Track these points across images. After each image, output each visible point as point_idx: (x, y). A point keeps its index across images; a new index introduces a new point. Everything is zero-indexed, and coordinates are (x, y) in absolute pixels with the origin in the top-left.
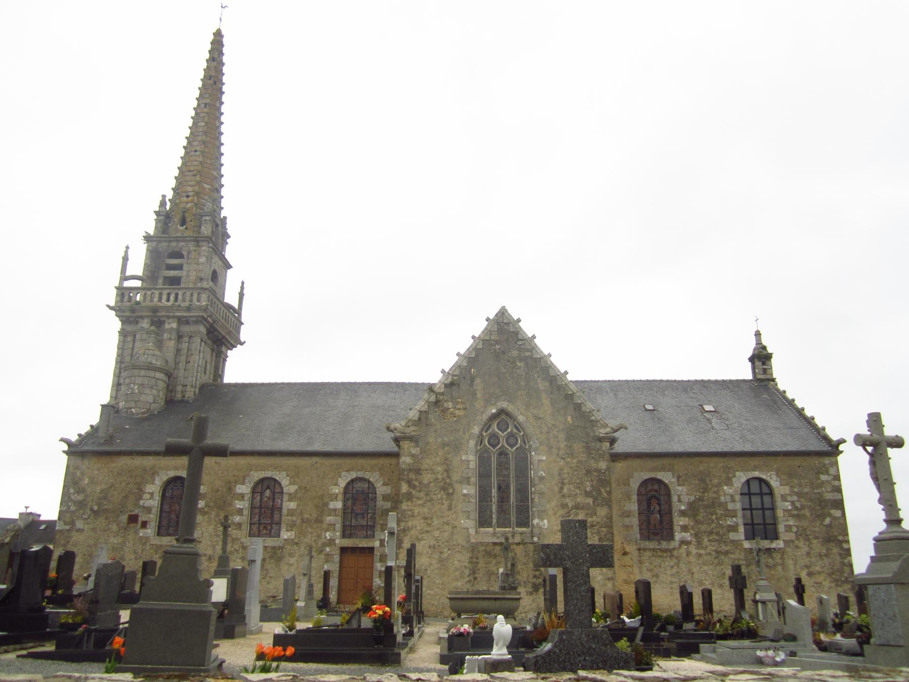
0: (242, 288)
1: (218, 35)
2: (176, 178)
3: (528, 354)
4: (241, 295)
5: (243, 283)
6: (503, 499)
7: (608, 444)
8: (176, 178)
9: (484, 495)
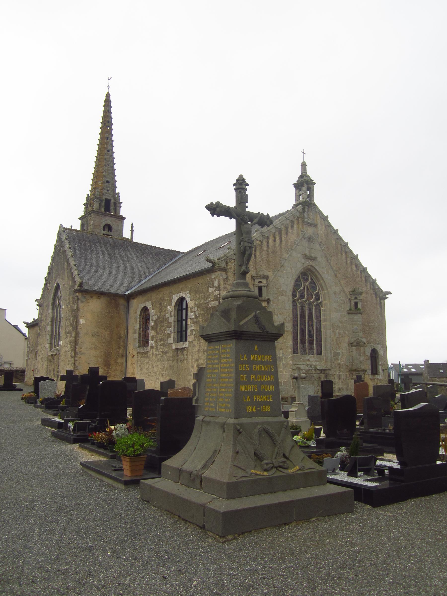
0: (132, 227)
1: (108, 96)
2: (100, 128)
3: (312, 375)
4: (132, 231)
5: (132, 224)
6: (303, 335)
7: (266, 303)
8: (100, 128)
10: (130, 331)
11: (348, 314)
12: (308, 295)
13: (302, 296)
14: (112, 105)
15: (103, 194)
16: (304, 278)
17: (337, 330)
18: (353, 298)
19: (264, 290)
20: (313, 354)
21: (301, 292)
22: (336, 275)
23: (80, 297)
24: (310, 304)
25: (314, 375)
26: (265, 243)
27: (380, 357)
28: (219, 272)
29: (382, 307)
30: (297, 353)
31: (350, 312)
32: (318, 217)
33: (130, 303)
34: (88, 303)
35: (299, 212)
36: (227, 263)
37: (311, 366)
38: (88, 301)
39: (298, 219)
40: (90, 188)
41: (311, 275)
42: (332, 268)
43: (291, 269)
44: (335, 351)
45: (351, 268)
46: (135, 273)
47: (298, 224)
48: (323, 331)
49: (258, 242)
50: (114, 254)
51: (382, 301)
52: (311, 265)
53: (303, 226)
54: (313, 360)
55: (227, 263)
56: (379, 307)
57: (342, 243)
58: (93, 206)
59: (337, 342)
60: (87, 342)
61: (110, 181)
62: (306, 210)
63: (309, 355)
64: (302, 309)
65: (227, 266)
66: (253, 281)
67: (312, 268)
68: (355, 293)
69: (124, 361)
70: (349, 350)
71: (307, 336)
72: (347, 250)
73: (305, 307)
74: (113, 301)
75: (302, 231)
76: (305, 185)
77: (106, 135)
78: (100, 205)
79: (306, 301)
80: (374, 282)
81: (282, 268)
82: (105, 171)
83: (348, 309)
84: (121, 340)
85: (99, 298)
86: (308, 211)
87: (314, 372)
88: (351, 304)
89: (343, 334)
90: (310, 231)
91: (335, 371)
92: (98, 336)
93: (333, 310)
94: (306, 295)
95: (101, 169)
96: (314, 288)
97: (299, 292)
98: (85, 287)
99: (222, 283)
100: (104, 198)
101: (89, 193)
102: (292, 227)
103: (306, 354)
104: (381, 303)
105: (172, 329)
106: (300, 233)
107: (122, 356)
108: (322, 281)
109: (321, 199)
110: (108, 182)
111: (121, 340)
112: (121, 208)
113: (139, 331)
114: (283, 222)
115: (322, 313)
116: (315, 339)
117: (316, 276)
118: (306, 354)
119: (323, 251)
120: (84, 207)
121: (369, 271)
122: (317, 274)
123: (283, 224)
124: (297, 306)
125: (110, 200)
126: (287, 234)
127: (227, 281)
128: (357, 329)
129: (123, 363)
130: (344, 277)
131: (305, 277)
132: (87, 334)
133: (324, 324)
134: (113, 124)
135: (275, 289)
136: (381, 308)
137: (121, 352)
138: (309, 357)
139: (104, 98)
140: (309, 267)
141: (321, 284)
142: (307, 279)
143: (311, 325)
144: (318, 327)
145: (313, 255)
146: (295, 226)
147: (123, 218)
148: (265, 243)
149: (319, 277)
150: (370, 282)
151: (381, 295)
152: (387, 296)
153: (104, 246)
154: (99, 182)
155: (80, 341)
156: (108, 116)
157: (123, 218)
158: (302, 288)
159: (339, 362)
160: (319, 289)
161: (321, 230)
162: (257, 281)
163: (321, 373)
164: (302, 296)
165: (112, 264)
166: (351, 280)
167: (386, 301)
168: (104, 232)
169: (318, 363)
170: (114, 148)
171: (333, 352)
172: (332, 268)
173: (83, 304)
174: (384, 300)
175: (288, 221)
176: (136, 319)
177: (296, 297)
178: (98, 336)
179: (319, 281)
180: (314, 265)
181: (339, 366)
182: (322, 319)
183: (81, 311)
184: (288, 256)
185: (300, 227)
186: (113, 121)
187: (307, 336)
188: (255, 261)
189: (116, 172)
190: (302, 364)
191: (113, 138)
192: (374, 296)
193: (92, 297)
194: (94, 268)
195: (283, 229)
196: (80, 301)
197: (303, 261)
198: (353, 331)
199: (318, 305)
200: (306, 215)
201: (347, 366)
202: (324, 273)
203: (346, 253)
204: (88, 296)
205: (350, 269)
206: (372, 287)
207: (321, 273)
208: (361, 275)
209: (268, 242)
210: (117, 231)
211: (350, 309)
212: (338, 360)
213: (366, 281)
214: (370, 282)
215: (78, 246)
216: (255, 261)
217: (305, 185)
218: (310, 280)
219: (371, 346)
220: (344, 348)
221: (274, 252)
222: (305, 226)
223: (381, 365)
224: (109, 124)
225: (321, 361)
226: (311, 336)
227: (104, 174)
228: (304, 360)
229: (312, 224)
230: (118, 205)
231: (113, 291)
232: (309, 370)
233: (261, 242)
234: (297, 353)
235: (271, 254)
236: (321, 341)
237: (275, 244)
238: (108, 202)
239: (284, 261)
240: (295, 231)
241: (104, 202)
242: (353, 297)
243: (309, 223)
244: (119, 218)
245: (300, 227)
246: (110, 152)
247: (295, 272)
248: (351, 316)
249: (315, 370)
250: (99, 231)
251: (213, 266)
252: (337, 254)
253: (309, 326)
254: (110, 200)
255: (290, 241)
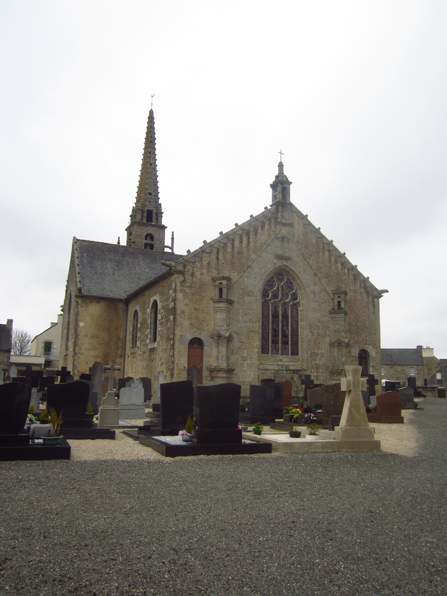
0: (173, 235)
1: (151, 112)
3: (282, 375)
4: (173, 239)
5: (173, 233)
6: (275, 335)
9: (264, 339)
10: (128, 333)
11: (331, 313)
12: (282, 295)
13: (275, 296)
14: (155, 121)
15: (145, 206)
16: (278, 278)
17: (315, 330)
18: (336, 297)
19: (224, 291)
20: (287, 354)
21: (274, 293)
22: (316, 274)
23: (79, 302)
24: (285, 304)
25: (285, 375)
26: (229, 245)
27: (371, 358)
28: (176, 275)
29: (376, 307)
30: (268, 353)
31: (333, 312)
32: (295, 216)
33: (129, 306)
34: (88, 307)
35: (272, 213)
36: (185, 266)
37: (282, 366)
38: (88, 305)
39: (270, 219)
40: (135, 200)
41: (286, 275)
42: (311, 267)
43: (260, 270)
44: (312, 351)
45: (336, 267)
46: (139, 279)
47: (270, 224)
48: (301, 331)
49: (221, 244)
50: (122, 261)
51: (376, 300)
52: (285, 265)
53: (275, 226)
54: (286, 361)
55: (185, 266)
56: (371, 306)
57: (325, 242)
58: (136, 218)
59: (315, 342)
60: (86, 343)
61: (153, 192)
62: (280, 210)
63: (282, 355)
64: (275, 308)
65: (184, 268)
66: (214, 282)
67: (286, 268)
68: (340, 293)
69: (123, 362)
70: (331, 350)
71: (280, 337)
72: (331, 248)
73: (279, 307)
74: (112, 305)
75: (274, 231)
76: (279, 185)
77: (149, 150)
78: (142, 216)
79: (280, 301)
80: (366, 281)
81: (250, 269)
82: (147, 184)
83: (331, 308)
84: (120, 342)
85: (99, 302)
86: (282, 211)
87: (285, 372)
88: (333, 303)
89: (324, 334)
90: (284, 231)
91: (311, 372)
92: (97, 337)
93: (312, 311)
94: (280, 295)
95: (144, 182)
96: (291, 288)
97: (271, 293)
98: (84, 293)
99: (179, 285)
100: (146, 209)
101: (134, 205)
102: (263, 227)
103: (279, 354)
104: (374, 302)
105: (148, 330)
106: (272, 233)
107: (121, 356)
108: (298, 281)
109: (296, 198)
110: (150, 194)
111: (120, 342)
112: (163, 218)
113: (133, 333)
114: (252, 224)
115: (299, 312)
116: (290, 339)
117: (291, 275)
118: (279, 354)
119: (299, 250)
120: (130, 218)
121: (359, 269)
122: (293, 274)
123: (251, 225)
124: (269, 306)
125: (152, 211)
126: (256, 235)
127: (184, 283)
128: (339, 329)
129: (121, 363)
130: (326, 276)
131: (280, 277)
132: (86, 336)
133: (301, 324)
134: (156, 139)
135: (241, 290)
136: (374, 307)
137: (119, 352)
138: (281, 357)
139: (148, 115)
140: (283, 267)
141: (298, 284)
142: (282, 279)
143: (285, 325)
144: (295, 327)
145: (287, 255)
146: (266, 227)
147: (164, 228)
148: (229, 245)
149: (295, 276)
150: (360, 281)
151: (375, 293)
152: (382, 294)
153: (114, 254)
154: (142, 195)
155: (79, 342)
156: (150, 132)
157: (164, 228)
158: (275, 288)
159: (317, 362)
160: (297, 288)
161: (298, 229)
162: (217, 282)
163: (294, 373)
164: (275, 296)
165: (118, 271)
166: (334, 278)
167: (381, 300)
168: (146, 241)
169: (292, 363)
170: (157, 162)
171: (309, 352)
172: (311, 267)
173: (83, 309)
174: (378, 299)
175: (258, 222)
176: (131, 322)
177: (268, 297)
178: (97, 337)
179: (296, 281)
180: (288, 264)
181: (317, 367)
182: (299, 319)
183: (81, 315)
184: (256, 257)
185: (273, 226)
186: (156, 136)
187: (280, 337)
188: (218, 263)
189: (159, 185)
190: (272, 363)
191: (157, 152)
192: (364, 295)
193: (91, 302)
194: (98, 275)
195: (252, 229)
196: (79, 306)
197: (275, 261)
198: (335, 331)
199: (294, 304)
200: (279, 215)
201: (328, 367)
202: (301, 272)
203: (329, 251)
204: (87, 301)
205: (334, 268)
206: (362, 285)
207: (297, 272)
208: (349, 273)
209: (233, 244)
210: (158, 240)
211: (333, 309)
212: (316, 360)
213: (355, 279)
214: (360, 281)
215: (87, 256)
216: (218, 263)
217: (279, 185)
218: (285, 280)
219: (359, 346)
220: (324, 348)
221: (240, 253)
222: (278, 226)
223: (372, 366)
224: (152, 139)
225: (297, 362)
226: (285, 335)
227: (146, 186)
228: (275, 360)
229: (286, 224)
230: (159, 215)
231: (112, 295)
232: (279, 370)
233: (225, 244)
234: (268, 353)
235: (236, 255)
236: (298, 341)
237: (241, 246)
238: (150, 213)
239: (252, 262)
240: (266, 232)
241: (147, 214)
242: (336, 296)
243: (282, 223)
244: (160, 228)
245: (273, 226)
246: (153, 166)
247: (265, 273)
248: (333, 316)
249: (287, 370)
250: (140, 240)
251: (170, 269)
252: (318, 253)
253: (283, 326)
254: (152, 211)
255: (259, 242)
